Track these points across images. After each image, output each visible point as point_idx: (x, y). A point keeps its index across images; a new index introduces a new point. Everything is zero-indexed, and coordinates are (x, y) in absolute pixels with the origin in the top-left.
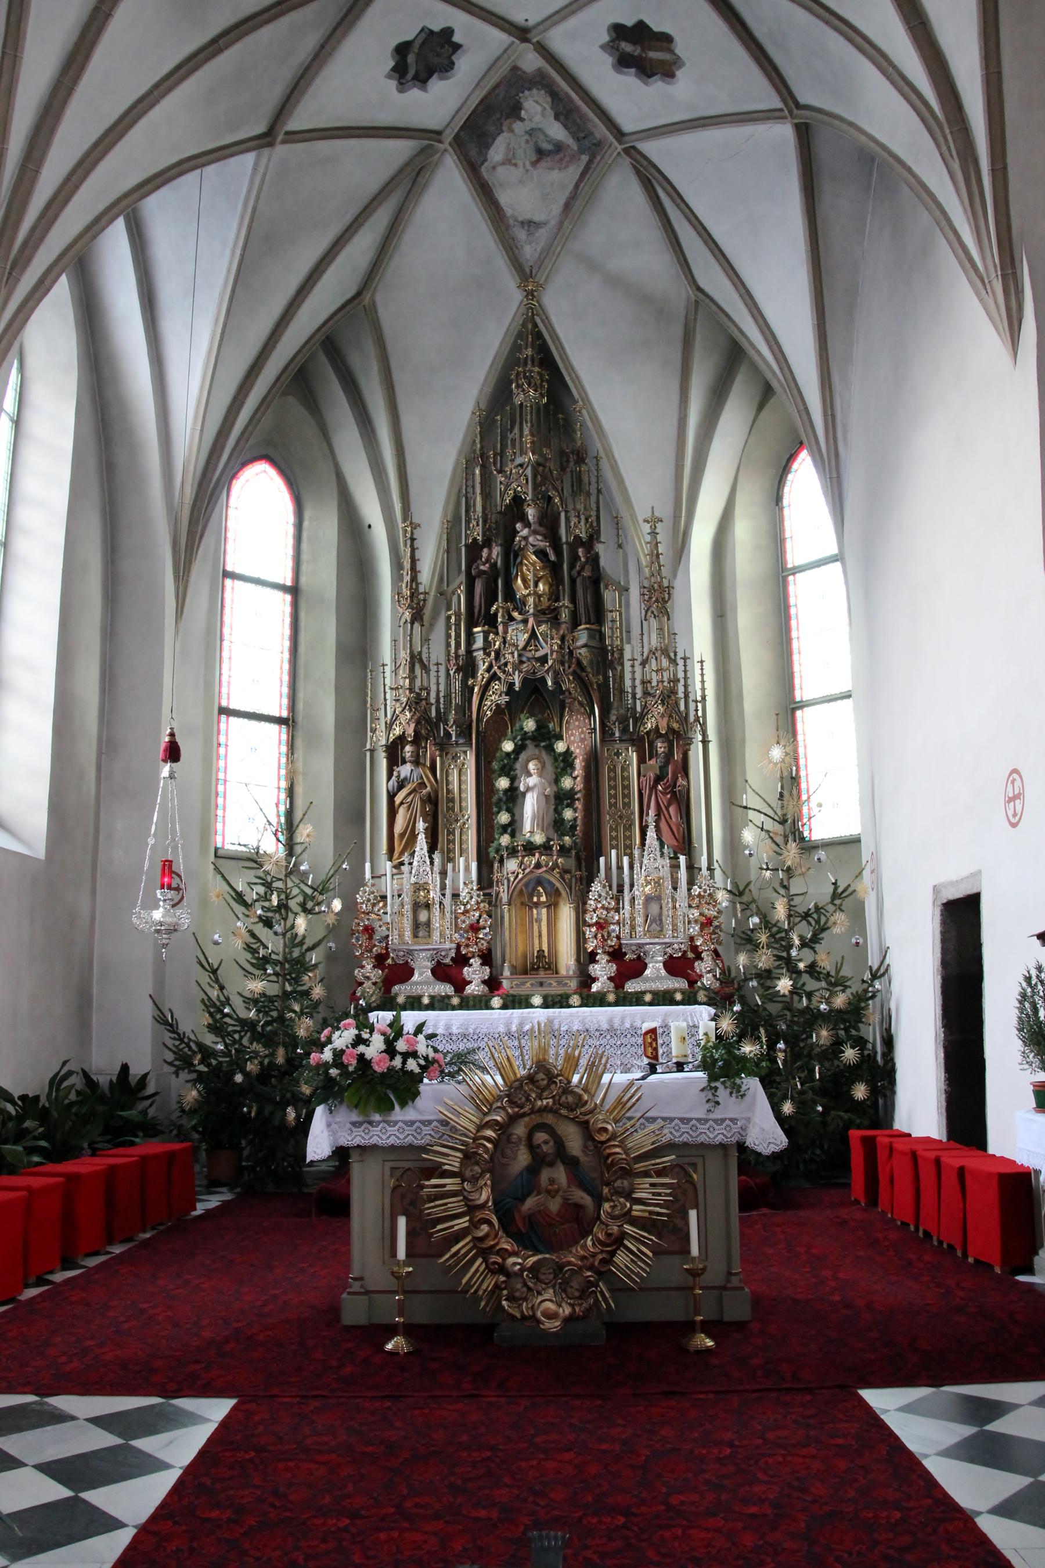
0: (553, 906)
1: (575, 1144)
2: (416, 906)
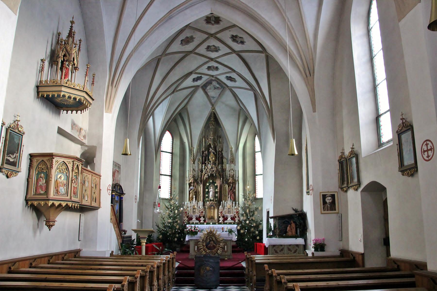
0: (214, 209)
1: (214, 239)
2: (193, 209)
